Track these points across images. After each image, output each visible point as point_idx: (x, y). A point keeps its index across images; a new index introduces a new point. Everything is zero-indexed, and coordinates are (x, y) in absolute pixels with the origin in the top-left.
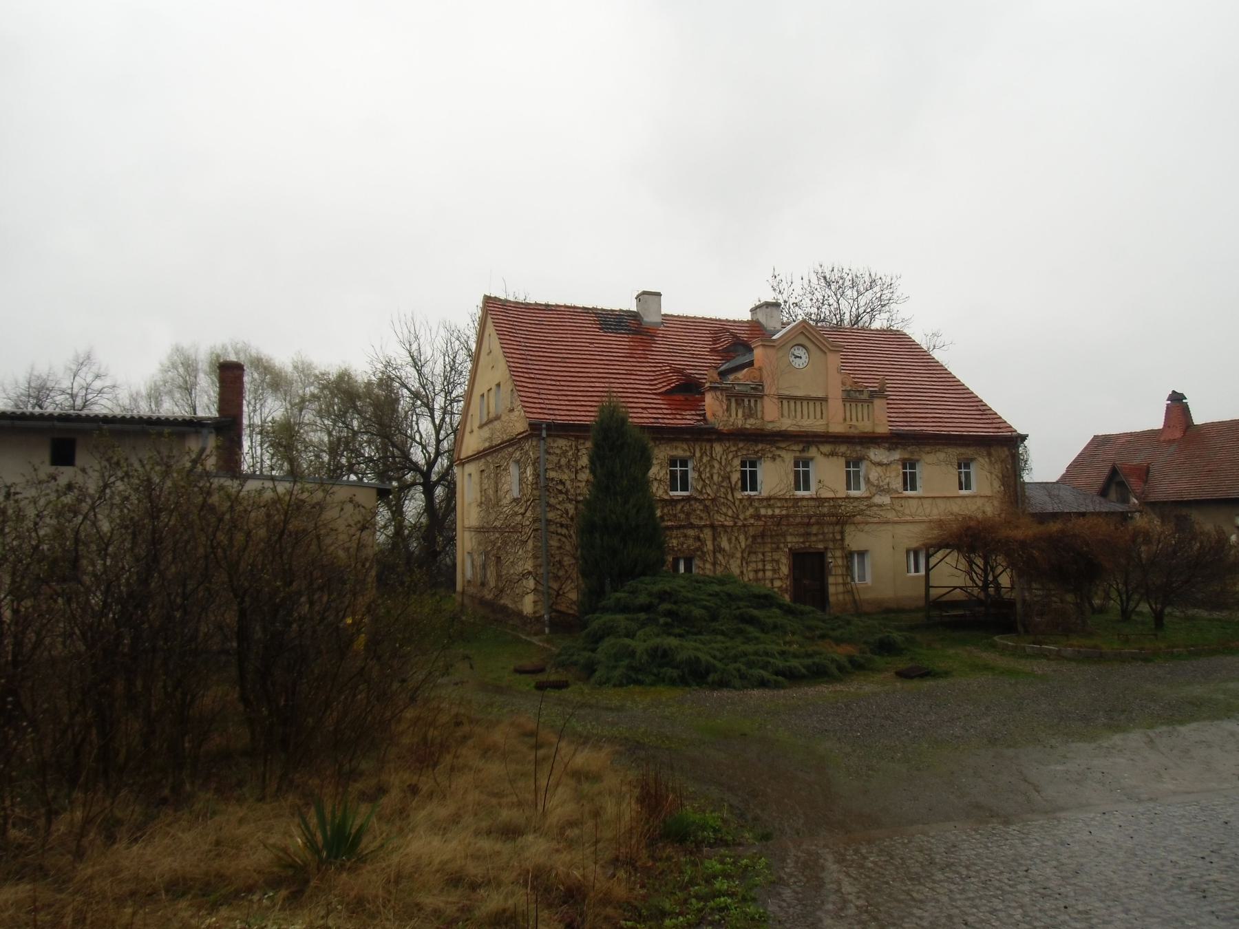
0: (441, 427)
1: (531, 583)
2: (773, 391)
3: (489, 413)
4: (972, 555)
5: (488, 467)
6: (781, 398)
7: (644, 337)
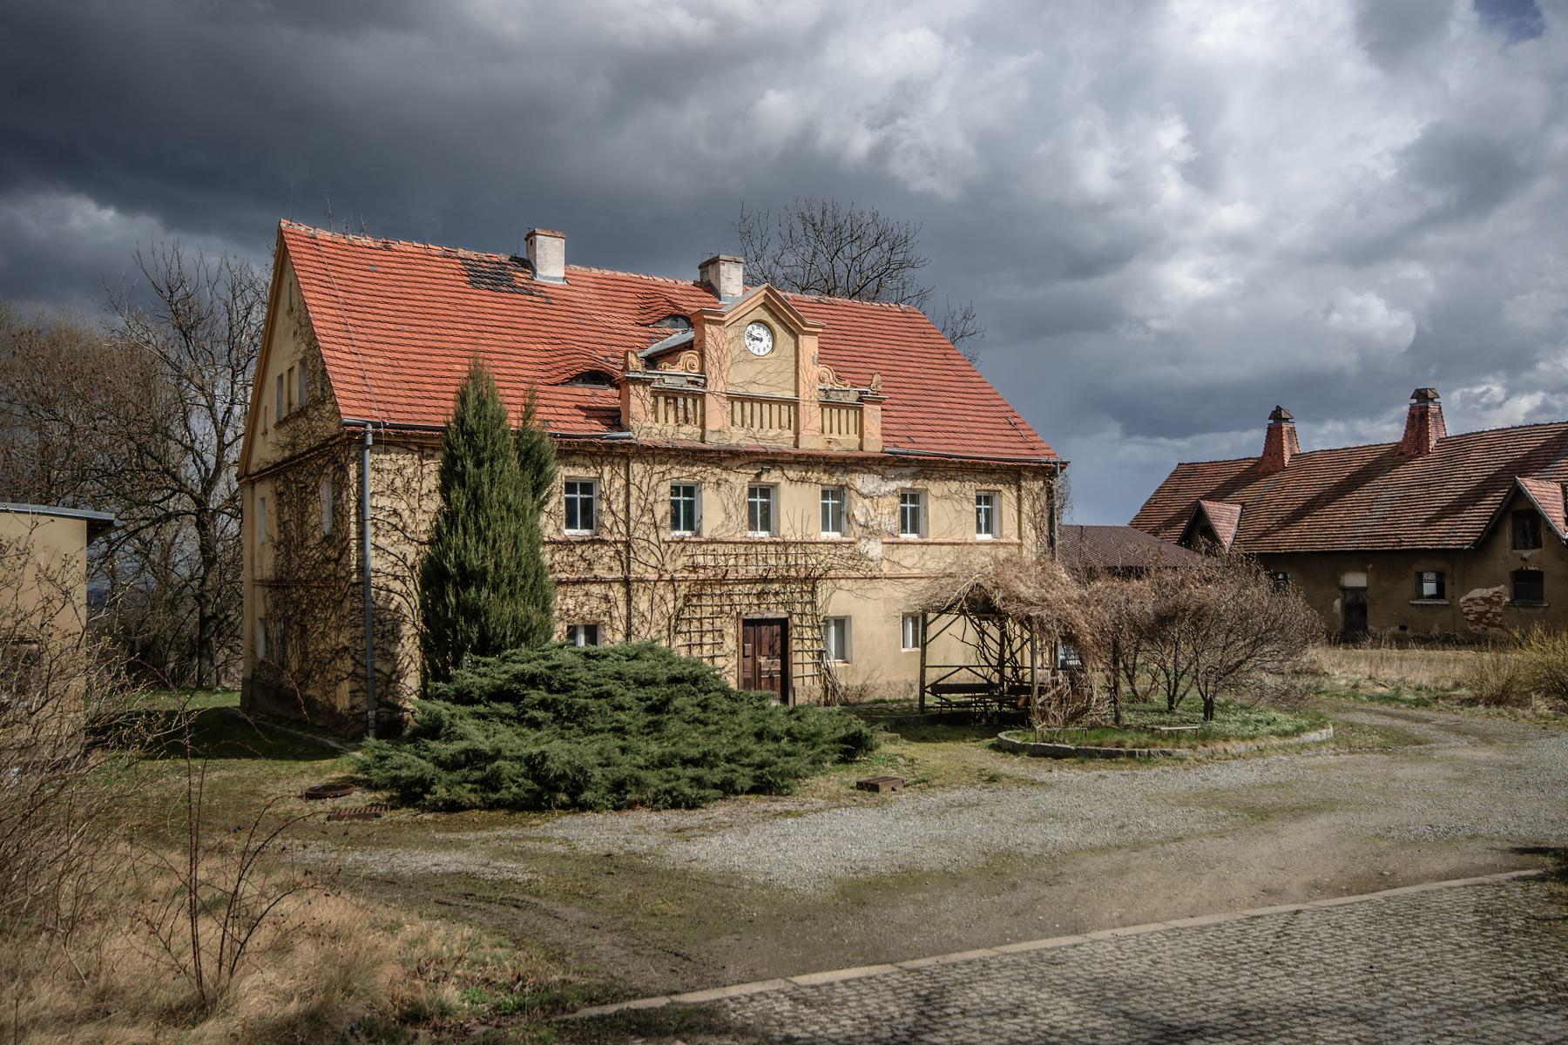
0: (225, 422)
1: (347, 665)
2: (721, 387)
3: (290, 404)
4: (985, 624)
5: (288, 487)
6: (732, 398)
7: (535, 299)
